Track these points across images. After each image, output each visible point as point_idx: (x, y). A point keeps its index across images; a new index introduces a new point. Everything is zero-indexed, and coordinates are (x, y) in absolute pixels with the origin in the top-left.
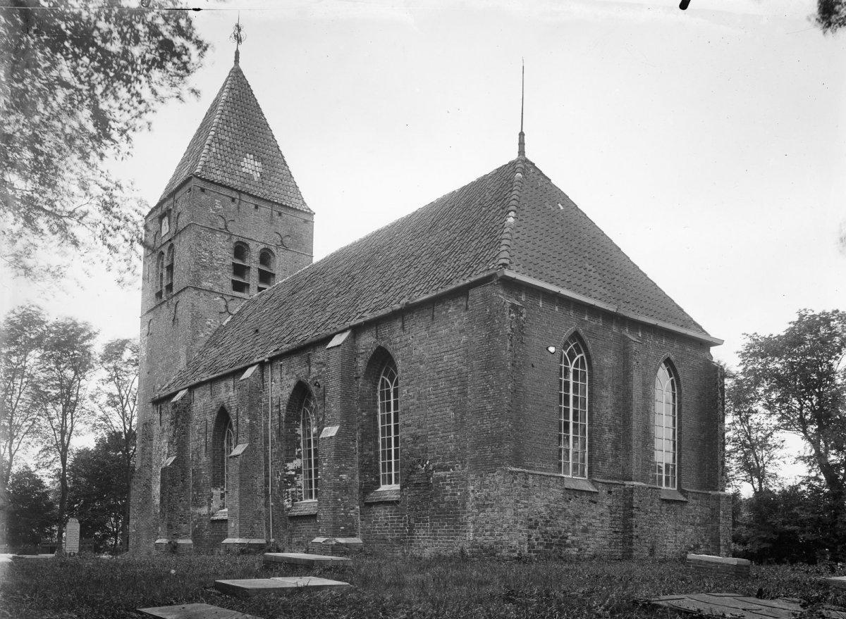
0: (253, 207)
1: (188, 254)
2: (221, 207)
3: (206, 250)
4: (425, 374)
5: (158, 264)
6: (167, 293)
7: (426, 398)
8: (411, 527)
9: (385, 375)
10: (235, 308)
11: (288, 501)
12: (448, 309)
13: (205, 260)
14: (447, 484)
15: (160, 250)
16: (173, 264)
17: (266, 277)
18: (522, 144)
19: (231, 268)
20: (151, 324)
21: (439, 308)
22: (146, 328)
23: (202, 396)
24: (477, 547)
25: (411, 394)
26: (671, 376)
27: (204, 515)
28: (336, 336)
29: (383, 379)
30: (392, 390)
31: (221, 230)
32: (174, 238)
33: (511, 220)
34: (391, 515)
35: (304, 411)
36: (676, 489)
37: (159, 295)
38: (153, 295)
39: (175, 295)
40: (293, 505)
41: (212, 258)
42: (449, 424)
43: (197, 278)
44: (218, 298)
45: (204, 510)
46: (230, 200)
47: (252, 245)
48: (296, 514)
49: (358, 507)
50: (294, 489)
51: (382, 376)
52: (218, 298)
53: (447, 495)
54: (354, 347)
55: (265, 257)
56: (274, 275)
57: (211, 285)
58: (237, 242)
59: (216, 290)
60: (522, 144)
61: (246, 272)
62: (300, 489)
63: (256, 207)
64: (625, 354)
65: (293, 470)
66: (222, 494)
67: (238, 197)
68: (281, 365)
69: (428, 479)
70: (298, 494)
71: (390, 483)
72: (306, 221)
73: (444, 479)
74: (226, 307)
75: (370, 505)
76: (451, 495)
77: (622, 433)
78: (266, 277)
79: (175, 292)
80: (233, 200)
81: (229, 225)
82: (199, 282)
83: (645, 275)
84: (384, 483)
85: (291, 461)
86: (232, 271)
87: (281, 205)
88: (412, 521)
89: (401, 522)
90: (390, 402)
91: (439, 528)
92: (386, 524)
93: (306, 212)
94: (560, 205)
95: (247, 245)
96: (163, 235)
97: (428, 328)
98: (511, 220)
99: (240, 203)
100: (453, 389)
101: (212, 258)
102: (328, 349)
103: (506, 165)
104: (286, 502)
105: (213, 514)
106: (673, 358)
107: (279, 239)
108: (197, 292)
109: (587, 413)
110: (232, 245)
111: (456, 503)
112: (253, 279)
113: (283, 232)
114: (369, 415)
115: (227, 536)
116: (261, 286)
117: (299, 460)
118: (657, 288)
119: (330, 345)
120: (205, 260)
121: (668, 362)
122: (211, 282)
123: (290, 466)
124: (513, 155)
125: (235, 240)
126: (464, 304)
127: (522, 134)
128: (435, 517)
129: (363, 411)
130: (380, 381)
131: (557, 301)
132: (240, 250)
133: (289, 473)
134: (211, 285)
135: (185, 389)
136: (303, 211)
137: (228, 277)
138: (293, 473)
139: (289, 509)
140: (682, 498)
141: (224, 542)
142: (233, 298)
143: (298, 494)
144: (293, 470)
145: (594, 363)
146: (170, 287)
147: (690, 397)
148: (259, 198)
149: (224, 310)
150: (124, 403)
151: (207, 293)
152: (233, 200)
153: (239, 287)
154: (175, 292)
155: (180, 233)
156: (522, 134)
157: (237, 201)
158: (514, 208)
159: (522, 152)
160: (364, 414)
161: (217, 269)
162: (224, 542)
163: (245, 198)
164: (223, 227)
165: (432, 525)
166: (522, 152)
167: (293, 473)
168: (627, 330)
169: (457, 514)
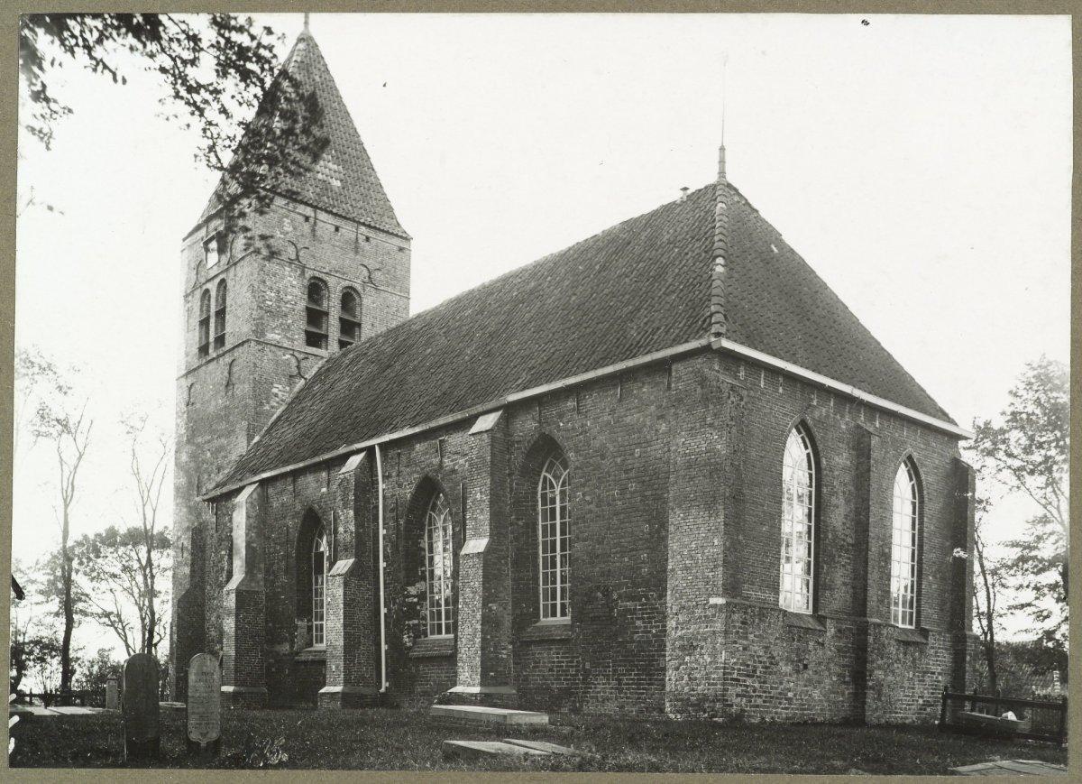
0: (333, 229)
1: (249, 295)
2: (291, 229)
3: (271, 289)
4: (608, 472)
5: (202, 306)
6: (216, 348)
7: (609, 505)
8: (587, 673)
9: (546, 471)
10: (312, 369)
11: (409, 637)
12: (641, 387)
13: (271, 303)
14: (638, 619)
15: (204, 288)
16: (225, 308)
17: (349, 327)
18: (722, 162)
19: (304, 314)
20: (192, 391)
21: (630, 385)
22: (185, 395)
23: (281, 493)
24: (682, 700)
25: (588, 498)
26: (911, 479)
27: (284, 655)
28: (480, 418)
29: (545, 478)
30: (557, 492)
31: (291, 262)
32: (227, 270)
33: (719, 269)
34: (558, 658)
35: (430, 519)
36: (913, 627)
37: (204, 350)
38: (195, 350)
39: (229, 351)
40: (414, 643)
41: (280, 300)
42: (641, 539)
43: (259, 331)
44: (288, 356)
45: (286, 648)
46: (301, 219)
47: (331, 281)
48: (421, 654)
49: (510, 647)
50: (416, 622)
51: (544, 473)
52: (288, 356)
53: (637, 633)
54: (508, 434)
55: (349, 298)
56: (359, 325)
57: (277, 337)
58: (311, 278)
59: (285, 345)
60: (722, 162)
61: (324, 319)
62: (424, 622)
63: (337, 229)
64: (861, 449)
65: (414, 596)
66: (308, 626)
67: (313, 215)
68: (399, 454)
69: (611, 610)
70: (422, 628)
71: (554, 614)
72: (401, 249)
73: (633, 612)
74: (298, 367)
75: (529, 644)
76: (642, 632)
77: (848, 549)
78: (349, 327)
79: (228, 346)
80: (307, 219)
81: (301, 254)
82: (263, 334)
83: (879, 344)
84: (546, 616)
85: (413, 584)
86: (306, 319)
87: (387, 232)
88: (588, 666)
89: (572, 667)
90: (555, 508)
91: (625, 675)
92: (551, 670)
93: (401, 237)
94: (773, 246)
95: (325, 283)
96: (209, 266)
97: (613, 411)
98: (719, 269)
99: (315, 223)
100: (646, 494)
101: (280, 300)
102: (473, 434)
103: (700, 190)
104: (406, 639)
105: (297, 654)
106: (915, 456)
107: (366, 274)
108: (260, 347)
109: (386, 438)
110: (306, 282)
111: (649, 642)
112: (333, 329)
113: (372, 264)
114: (527, 525)
115: (455, 684)
116: (345, 339)
117: (423, 583)
118: (894, 361)
119: (475, 429)
120: (271, 303)
121: (803, 427)
122: (279, 334)
123: (412, 590)
124: (712, 179)
125: (309, 274)
126: (666, 381)
127: (722, 149)
128: (621, 661)
129: (518, 519)
130: (541, 480)
131: (781, 380)
132: (315, 289)
133: (410, 600)
134: (277, 337)
135: (254, 483)
136: (397, 235)
137: (300, 325)
138: (416, 600)
139: (410, 648)
140: (918, 639)
141: (322, 691)
142: (307, 356)
143: (422, 628)
144: (414, 596)
145: (824, 461)
146: (220, 340)
147: (934, 507)
148: (340, 216)
149: (295, 373)
150: (145, 500)
151: (272, 348)
152: (307, 219)
153: (315, 339)
154: (228, 346)
155: (235, 264)
156: (722, 149)
157: (312, 220)
158: (721, 252)
159: (722, 173)
160: (520, 523)
161: (286, 316)
162: (322, 691)
163: (322, 216)
164: (293, 257)
165: (615, 671)
166: (722, 173)
167: (416, 600)
168: (832, 404)
169: (652, 659)
